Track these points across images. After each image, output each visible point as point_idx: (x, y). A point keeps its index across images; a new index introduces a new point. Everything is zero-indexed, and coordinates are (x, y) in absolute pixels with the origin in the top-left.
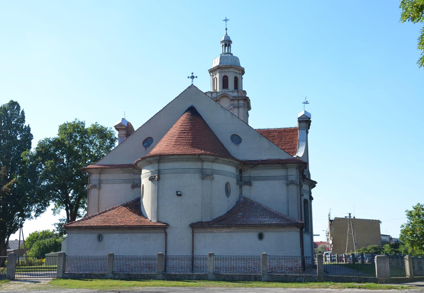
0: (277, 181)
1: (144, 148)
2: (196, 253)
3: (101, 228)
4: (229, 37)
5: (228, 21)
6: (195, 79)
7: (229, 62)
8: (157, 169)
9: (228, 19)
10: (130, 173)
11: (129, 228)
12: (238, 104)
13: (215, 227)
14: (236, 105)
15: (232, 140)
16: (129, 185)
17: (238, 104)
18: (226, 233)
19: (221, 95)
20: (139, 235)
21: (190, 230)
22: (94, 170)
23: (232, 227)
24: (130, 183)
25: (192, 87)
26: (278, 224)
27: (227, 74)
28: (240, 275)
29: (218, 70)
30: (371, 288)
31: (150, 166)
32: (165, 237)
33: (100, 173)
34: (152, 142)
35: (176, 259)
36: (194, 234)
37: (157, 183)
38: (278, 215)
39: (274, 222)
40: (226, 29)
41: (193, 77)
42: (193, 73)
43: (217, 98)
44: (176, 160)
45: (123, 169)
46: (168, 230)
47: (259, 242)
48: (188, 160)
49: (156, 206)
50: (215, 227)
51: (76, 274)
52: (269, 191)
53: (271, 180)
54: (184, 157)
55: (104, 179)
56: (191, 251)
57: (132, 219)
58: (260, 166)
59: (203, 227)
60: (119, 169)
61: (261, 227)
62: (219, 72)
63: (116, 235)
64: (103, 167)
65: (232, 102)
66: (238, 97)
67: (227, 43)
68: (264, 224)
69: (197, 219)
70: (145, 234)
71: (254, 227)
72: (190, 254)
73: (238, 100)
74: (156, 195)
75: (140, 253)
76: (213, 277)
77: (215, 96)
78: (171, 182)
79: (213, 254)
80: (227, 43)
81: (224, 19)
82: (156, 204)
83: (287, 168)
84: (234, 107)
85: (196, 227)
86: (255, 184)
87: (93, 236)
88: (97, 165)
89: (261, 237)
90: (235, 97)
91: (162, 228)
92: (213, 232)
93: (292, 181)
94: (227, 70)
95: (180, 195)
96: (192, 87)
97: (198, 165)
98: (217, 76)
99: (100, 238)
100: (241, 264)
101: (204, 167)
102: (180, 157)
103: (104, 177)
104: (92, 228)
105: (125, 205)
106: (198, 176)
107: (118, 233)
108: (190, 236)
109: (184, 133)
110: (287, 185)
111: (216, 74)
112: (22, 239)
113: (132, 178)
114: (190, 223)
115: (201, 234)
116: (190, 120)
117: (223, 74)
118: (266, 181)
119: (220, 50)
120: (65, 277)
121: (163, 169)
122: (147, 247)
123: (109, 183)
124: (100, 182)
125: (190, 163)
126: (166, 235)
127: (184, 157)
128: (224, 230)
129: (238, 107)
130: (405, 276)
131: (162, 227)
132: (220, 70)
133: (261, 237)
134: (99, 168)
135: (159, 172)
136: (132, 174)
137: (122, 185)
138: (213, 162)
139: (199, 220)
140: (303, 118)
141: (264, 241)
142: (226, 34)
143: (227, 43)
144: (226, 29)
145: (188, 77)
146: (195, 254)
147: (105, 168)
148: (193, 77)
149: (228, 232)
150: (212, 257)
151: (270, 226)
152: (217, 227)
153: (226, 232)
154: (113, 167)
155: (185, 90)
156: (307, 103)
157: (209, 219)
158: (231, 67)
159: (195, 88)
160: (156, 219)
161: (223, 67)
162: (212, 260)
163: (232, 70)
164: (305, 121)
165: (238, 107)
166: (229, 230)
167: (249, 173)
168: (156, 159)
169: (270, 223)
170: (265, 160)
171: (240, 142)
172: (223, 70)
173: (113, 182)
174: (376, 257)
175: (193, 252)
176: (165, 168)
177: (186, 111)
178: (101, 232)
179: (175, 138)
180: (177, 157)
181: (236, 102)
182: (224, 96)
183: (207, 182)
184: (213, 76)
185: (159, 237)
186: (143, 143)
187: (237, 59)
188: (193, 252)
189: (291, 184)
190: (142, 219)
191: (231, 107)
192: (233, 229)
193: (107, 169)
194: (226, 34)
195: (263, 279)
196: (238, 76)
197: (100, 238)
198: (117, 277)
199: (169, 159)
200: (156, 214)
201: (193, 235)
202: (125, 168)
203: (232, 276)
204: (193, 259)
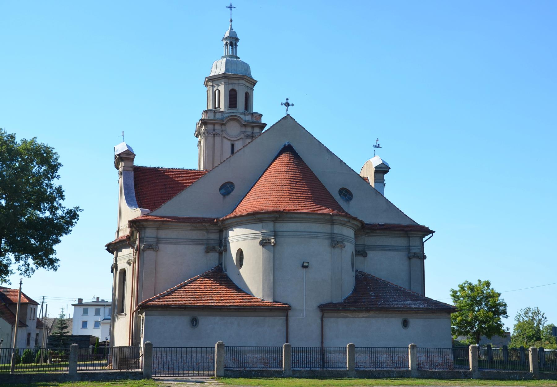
0: (396, 253)
1: (222, 196)
2: (327, 344)
3: (167, 307)
4: (235, 32)
5: (233, 9)
7: (240, 72)
8: (272, 230)
9: (233, 6)
10: (202, 230)
11: (236, 309)
12: (253, 133)
13: (351, 310)
14: (249, 134)
15: (340, 195)
16: (203, 247)
17: (253, 133)
18: (364, 319)
19: (229, 117)
20: (251, 320)
21: (319, 314)
22: (151, 223)
23: (372, 311)
24: (202, 244)
25: (288, 118)
26: (427, 308)
27: (236, 88)
28: (448, 372)
29: (223, 81)
30: (387, 384)
31: (260, 225)
32: (285, 322)
33: (158, 228)
34: (233, 190)
35: (303, 352)
36: (324, 319)
37: (272, 249)
38: (418, 297)
39: (421, 306)
40: (231, 21)
42: (287, 99)
43: (222, 120)
44: (302, 220)
45: (195, 225)
46: (290, 313)
47: (404, 331)
48: (316, 221)
49: (272, 280)
50: (351, 310)
51: (243, 372)
52: (384, 264)
53: (390, 250)
54: (313, 217)
55: (164, 236)
56: (320, 341)
57: (222, 296)
58: (378, 232)
59: (335, 310)
60: (188, 224)
61: (407, 311)
62: (225, 84)
63: (218, 318)
64: (162, 219)
65: (243, 129)
66: (253, 122)
67: (234, 42)
68: (410, 308)
69: (325, 299)
70: (258, 318)
71: (399, 311)
72: (319, 345)
73: (253, 127)
74: (272, 265)
75: (252, 343)
76: (417, 374)
77: (220, 118)
78: (293, 249)
79: (415, 346)
80: (233, 41)
81: (229, 5)
82: (272, 278)
83: (409, 237)
84: (247, 136)
85: (327, 309)
86: (371, 254)
87: (183, 321)
88: (154, 216)
89: (405, 324)
90: (248, 122)
91: (281, 310)
92: (348, 317)
93: (415, 253)
94: (236, 82)
95: (306, 267)
96: (288, 118)
97: (326, 228)
98: (222, 88)
99: (194, 322)
100: (382, 358)
101: (335, 232)
102: (308, 216)
103: (163, 234)
104: (183, 308)
105: (207, 276)
106: (327, 242)
107: (220, 316)
108: (319, 321)
109: (297, 182)
110: (409, 258)
111: (218, 85)
113: (205, 238)
114: (318, 304)
115: (332, 320)
116: (296, 164)
117: (231, 87)
118: (383, 252)
119: (223, 50)
120: (226, 376)
121: (281, 230)
122: (261, 334)
123: (171, 243)
124: (158, 240)
125: (318, 225)
126: (287, 320)
127: (313, 217)
128: (361, 315)
130: (469, 369)
131: (283, 309)
132: (227, 80)
133: (405, 324)
134: (152, 220)
136: (205, 233)
137: (191, 246)
138: (343, 225)
139: (329, 301)
140: (381, 168)
141: (410, 329)
143: (233, 41)
144: (231, 21)
145: (282, 104)
146: (324, 346)
147: (169, 221)
148: (287, 105)
149: (366, 317)
150: (416, 350)
151: (417, 311)
152: (354, 310)
153: (363, 317)
154: (178, 220)
155: (279, 122)
156: (378, 146)
157: (340, 300)
158: (243, 79)
159: (291, 120)
160: (272, 298)
161: (232, 76)
162: (415, 352)
163: (243, 82)
165: (252, 137)
166: (367, 315)
167: (370, 240)
168: (356, 225)
169: (417, 307)
170: (383, 225)
171: (351, 199)
172: (230, 81)
173: (177, 241)
174: (470, 347)
175: (322, 342)
176: (285, 230)
178: (195, 314)
179: (286, 189)
180: (304, 216)
181: (249, 130)
182: (234, 119)
183: (337, 250)
184: (213, 86)
185: (277, 322)
186: (221, 189)
187: (246, 67)
188: (322, 342)
189: (414, 256)
190: (248, 297)
191: (242, 136)
192: (372, 314)
193: (170, 223)
194: (231, 29)
195: (474, 376)
196: (249, 91)
197: (194, 322)
198: (297, 375)
199: (292, 218)
200: (272, 291)
201: (322, 321)
202: (198, 222)
203: (439, 373)
204: (323, 351)
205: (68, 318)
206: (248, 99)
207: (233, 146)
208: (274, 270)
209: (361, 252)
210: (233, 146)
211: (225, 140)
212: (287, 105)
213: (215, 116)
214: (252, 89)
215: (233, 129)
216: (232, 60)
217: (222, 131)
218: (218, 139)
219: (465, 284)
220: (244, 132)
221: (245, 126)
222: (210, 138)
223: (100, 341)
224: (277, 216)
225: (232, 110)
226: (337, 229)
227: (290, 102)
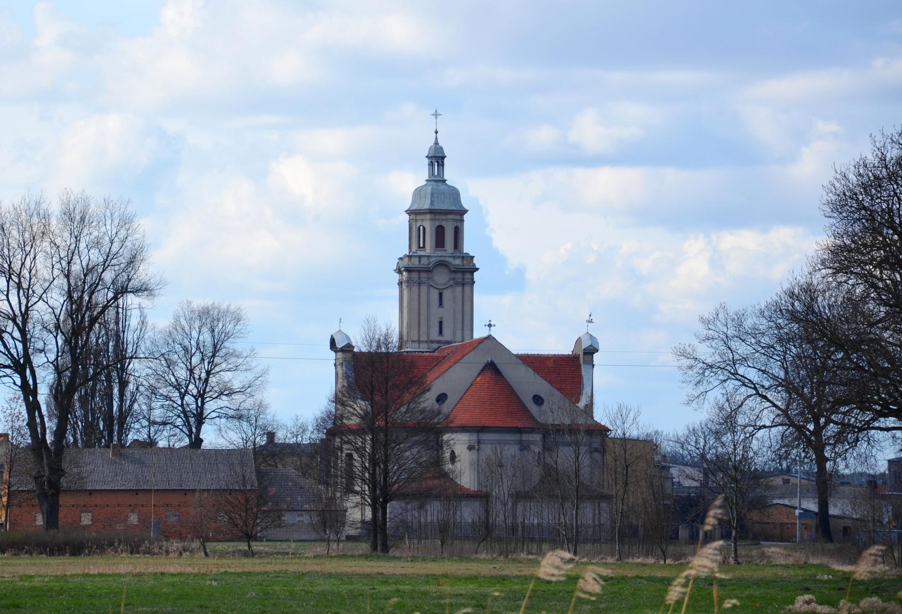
4: (441, 148)
6: (492, 328)
27: (444, 224)
29: (428, 216)
40: (436, 132)
41: (490, 326)
65: (453, 275)
80: (437, 159)
84: (457, 284)
85: (518, 496)
94: (444, 217)
98: (428, 225)
112: (597, 523)
117: (437, 223)
129: (463, 284)
132: (433, 216)
135: (479, 442)
142: (436, 143)
143: (437, 159)
144: (436, 132)
156: (591, 321)
164: (591, 351)
172: (437, 217)
177: (482, 370)
181: (459, 276)
194: (436, 143)
196: (459, 224)
205: (60, 503)
206: (458, 233)
207: (441, 294)
208: (483, 469)
209: (547, 448)
210: (441, 294)
211: (431, 289)
212: (490, 326)
213: (420, 261)
214: (462, 221)
215: (441, 277)
216: (437, 179)
217: (429, 278)
218: (424, 289)
219: (718, 434)
220: (454, 279)
221: (455, 272)
222: (415, 289)
223: (816, 510)
224: (480, 429)
225: (439, 253)
226: (525, 437)
227: (492, 323)
